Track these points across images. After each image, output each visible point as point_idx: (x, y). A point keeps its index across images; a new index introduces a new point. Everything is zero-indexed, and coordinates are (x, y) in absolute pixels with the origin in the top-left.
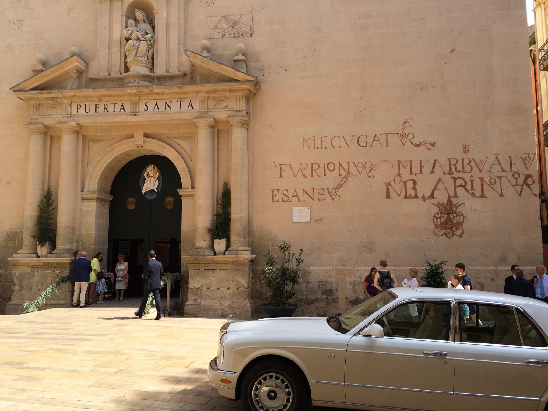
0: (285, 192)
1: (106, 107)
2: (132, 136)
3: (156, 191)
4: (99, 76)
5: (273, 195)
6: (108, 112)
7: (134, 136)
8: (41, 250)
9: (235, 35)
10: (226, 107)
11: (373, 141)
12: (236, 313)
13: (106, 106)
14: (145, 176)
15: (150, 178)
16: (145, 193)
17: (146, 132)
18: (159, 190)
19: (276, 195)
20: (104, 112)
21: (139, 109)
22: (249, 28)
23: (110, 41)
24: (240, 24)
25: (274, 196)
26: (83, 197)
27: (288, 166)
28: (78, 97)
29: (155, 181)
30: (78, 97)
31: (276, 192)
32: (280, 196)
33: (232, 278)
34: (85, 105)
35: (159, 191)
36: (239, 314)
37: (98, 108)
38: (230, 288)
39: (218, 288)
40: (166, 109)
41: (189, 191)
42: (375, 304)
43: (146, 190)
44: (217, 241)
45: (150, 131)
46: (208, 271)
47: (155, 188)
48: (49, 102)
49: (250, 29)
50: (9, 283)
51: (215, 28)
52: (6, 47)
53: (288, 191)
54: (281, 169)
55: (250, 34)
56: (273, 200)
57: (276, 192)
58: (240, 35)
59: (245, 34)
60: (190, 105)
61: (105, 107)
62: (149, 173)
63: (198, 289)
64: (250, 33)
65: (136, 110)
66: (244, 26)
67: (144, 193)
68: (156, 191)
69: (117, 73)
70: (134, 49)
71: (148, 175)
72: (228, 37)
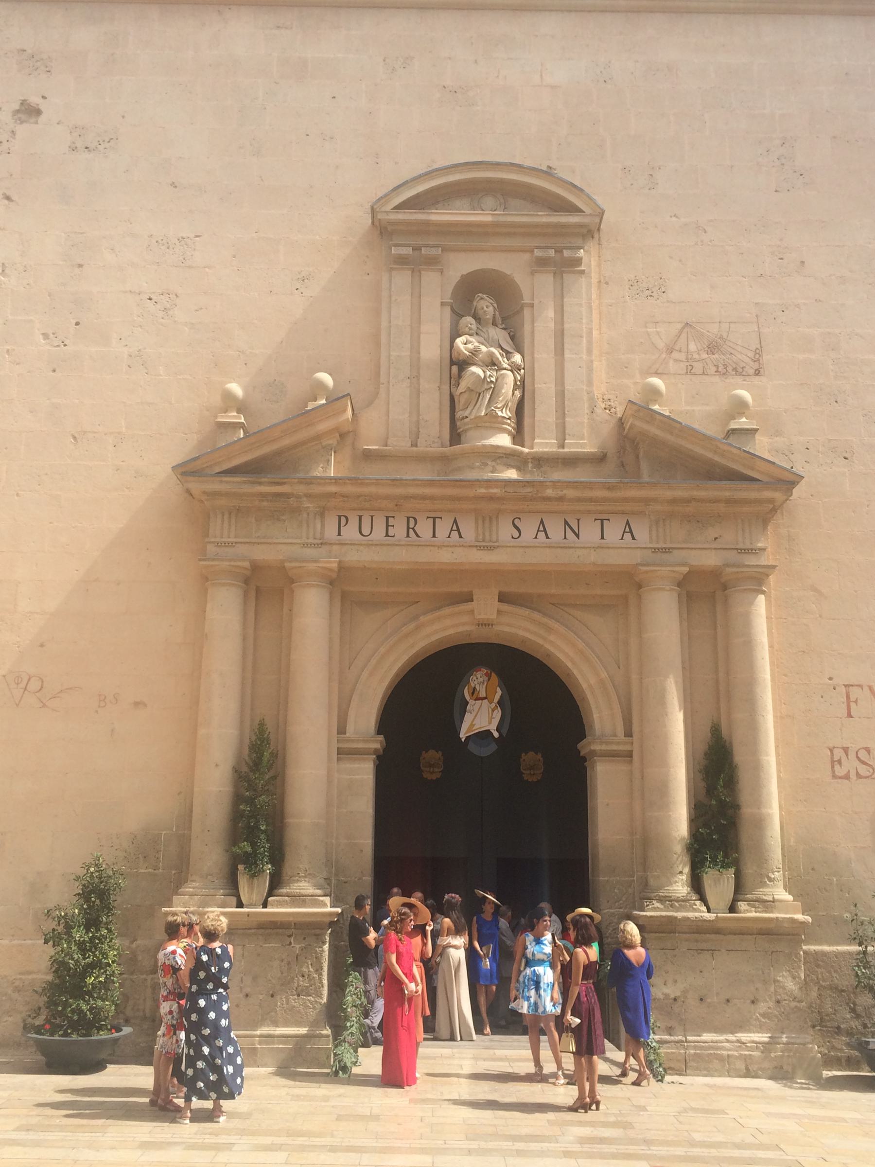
0: (863, 755)
1: (412, 525)
2: (468, 598)
3: (496, 735)
4: (388, 448)
5: (833, 762)
6: (418, 536)
7: (475, 598)
8: (251, 887)
9: (718, 368)
10: (716, 539)
11: (537, 533)
12: (782, 1067)
13: (412, 521)
14: (467, 696)
15: (480, 701)
16: (468, 738)
17: (505, 589)
18: (505, 731)
19: (840, 762)
20: (408, 536)
21: (497, 534)
22: (751, 354)
23: (416, 364)
24: (731, 345)
25: (835, 762)
26: (341, 748)
27: (866, 689)
28: (343, 496)
29: (493, 711)
30: (343, 496)
31: (838, 754)
32: (850, 765)
33: (763, 973)
34: (360, 517)
35: (504, 735)
36: (790, 1070)
37: (393, 526)
38: (757, 1000)
39: (728, 1001)
40: (565, 538)
41: (618, 743)
42: (771, 1044)
43: (469, 730)
44: (713, 875)
45: (513, 589)
46: (698, 954)
47: (493, 727)
48: (265, 504)
49: (754, 357)
50: (142, 974)
51: (670, 350)
52: (130, 356)
53: (869, 752)
54: (848, 697)
55: (756, 370)
56: (833, 772)
57: (838, 754)
58: (730, 369)
59: (742, 368)
60: (627, 530)
61: (411, 526)
62: (478, 687)
63: (675, 999)
64: (756, 366)
65: (490, 535)
66: (739, 349)
67: (463, 740)
68: (496, 735)
69: (434, 442)
70: (487, 390)
71: (473, 693)
72: (701, 372)
